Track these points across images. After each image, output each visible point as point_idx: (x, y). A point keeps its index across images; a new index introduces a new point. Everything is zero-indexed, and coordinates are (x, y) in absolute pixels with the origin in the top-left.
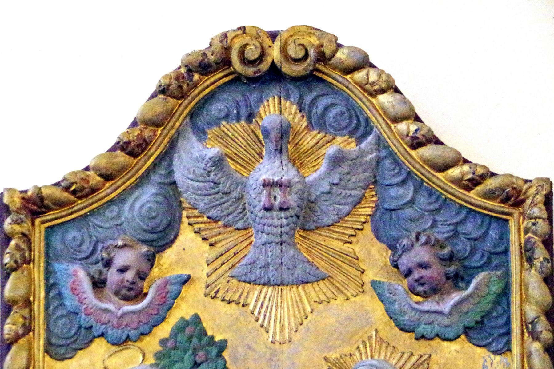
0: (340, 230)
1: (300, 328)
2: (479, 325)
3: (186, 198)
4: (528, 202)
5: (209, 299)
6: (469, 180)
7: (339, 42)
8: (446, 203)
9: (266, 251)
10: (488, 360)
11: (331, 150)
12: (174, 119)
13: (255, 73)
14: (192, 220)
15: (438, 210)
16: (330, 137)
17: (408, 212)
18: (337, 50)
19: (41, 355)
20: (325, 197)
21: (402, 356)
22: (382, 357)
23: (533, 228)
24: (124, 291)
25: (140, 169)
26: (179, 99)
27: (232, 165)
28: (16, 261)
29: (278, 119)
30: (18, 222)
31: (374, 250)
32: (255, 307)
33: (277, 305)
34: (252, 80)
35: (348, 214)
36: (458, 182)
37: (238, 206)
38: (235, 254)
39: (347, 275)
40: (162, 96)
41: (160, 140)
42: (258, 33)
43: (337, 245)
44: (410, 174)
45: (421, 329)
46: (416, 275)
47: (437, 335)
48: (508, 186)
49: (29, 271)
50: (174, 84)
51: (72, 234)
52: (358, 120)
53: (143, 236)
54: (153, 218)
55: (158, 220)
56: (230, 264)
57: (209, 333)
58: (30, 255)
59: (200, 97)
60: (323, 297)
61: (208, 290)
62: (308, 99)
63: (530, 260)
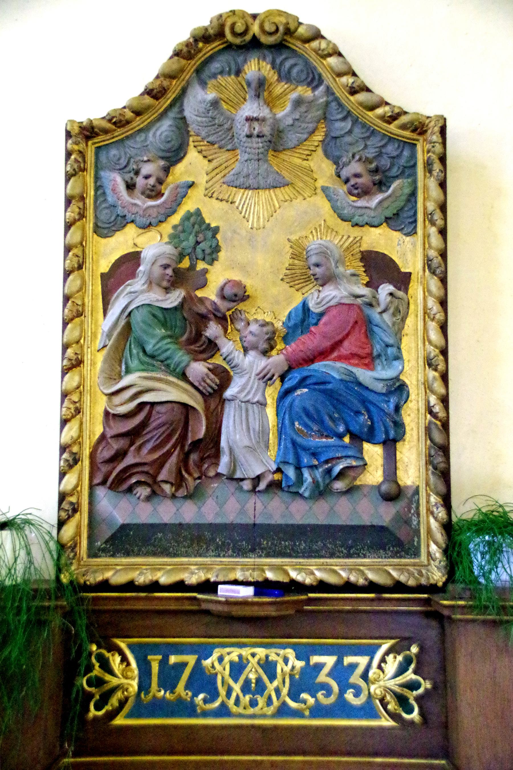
0: (301, 151)
1: (271, 219)
2: (396, 217)
3: (192, 128)
4: (429, 132)
5: (207, 199)
6: (390, 117)
7: (300, 21)
8: (373, 132)
9: (248, 166)
10: (401, 240)
11: (294, 95)
12: (185, 74)
13: (241, 42)
14: (196, 144)
15: (368, 137)
16: (292, 87)
17: (348, 139)
18: (298, 26)
19: (91, 234)
20: (290, 128)
21: (342, 238)
22: (328, 239)
23: (433, 149)
24: (148, 192)
25: (161, 107)
26: (188, 60)
27: (225, 106)
28: (74, 170)
29: (257, 75)
30: (77, 143)
31: (324, 165)
32: (239, 204)
33: (255, 203)
34: (240, 47)
35: (306, 140)
36: (382, 118)
37: (228, 135)
38: (226, 168)
39: (304, 182)
40: (176, 58)
41: (174, 89)
42: (243, 14)
43: (298, 161)
44: (349, 112)
45: (356, 219)
46: (353, 182)
47: (367, 224)
48: (416, 120)
49: (84, 177)
50: (185, 49)
51: (113, 152)
52: (314, 76)
53: (161, 154)
54: (169, 142)
55: (173, 143)
56: (222, 174)
57: (207, 221)
58: (84, 165)
59: (203, 59)
60: (287, 198)
61: (207, 191)
62: (278, 61)
63: (430, 172)
